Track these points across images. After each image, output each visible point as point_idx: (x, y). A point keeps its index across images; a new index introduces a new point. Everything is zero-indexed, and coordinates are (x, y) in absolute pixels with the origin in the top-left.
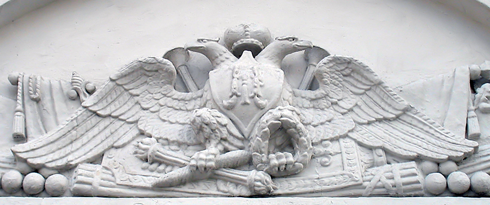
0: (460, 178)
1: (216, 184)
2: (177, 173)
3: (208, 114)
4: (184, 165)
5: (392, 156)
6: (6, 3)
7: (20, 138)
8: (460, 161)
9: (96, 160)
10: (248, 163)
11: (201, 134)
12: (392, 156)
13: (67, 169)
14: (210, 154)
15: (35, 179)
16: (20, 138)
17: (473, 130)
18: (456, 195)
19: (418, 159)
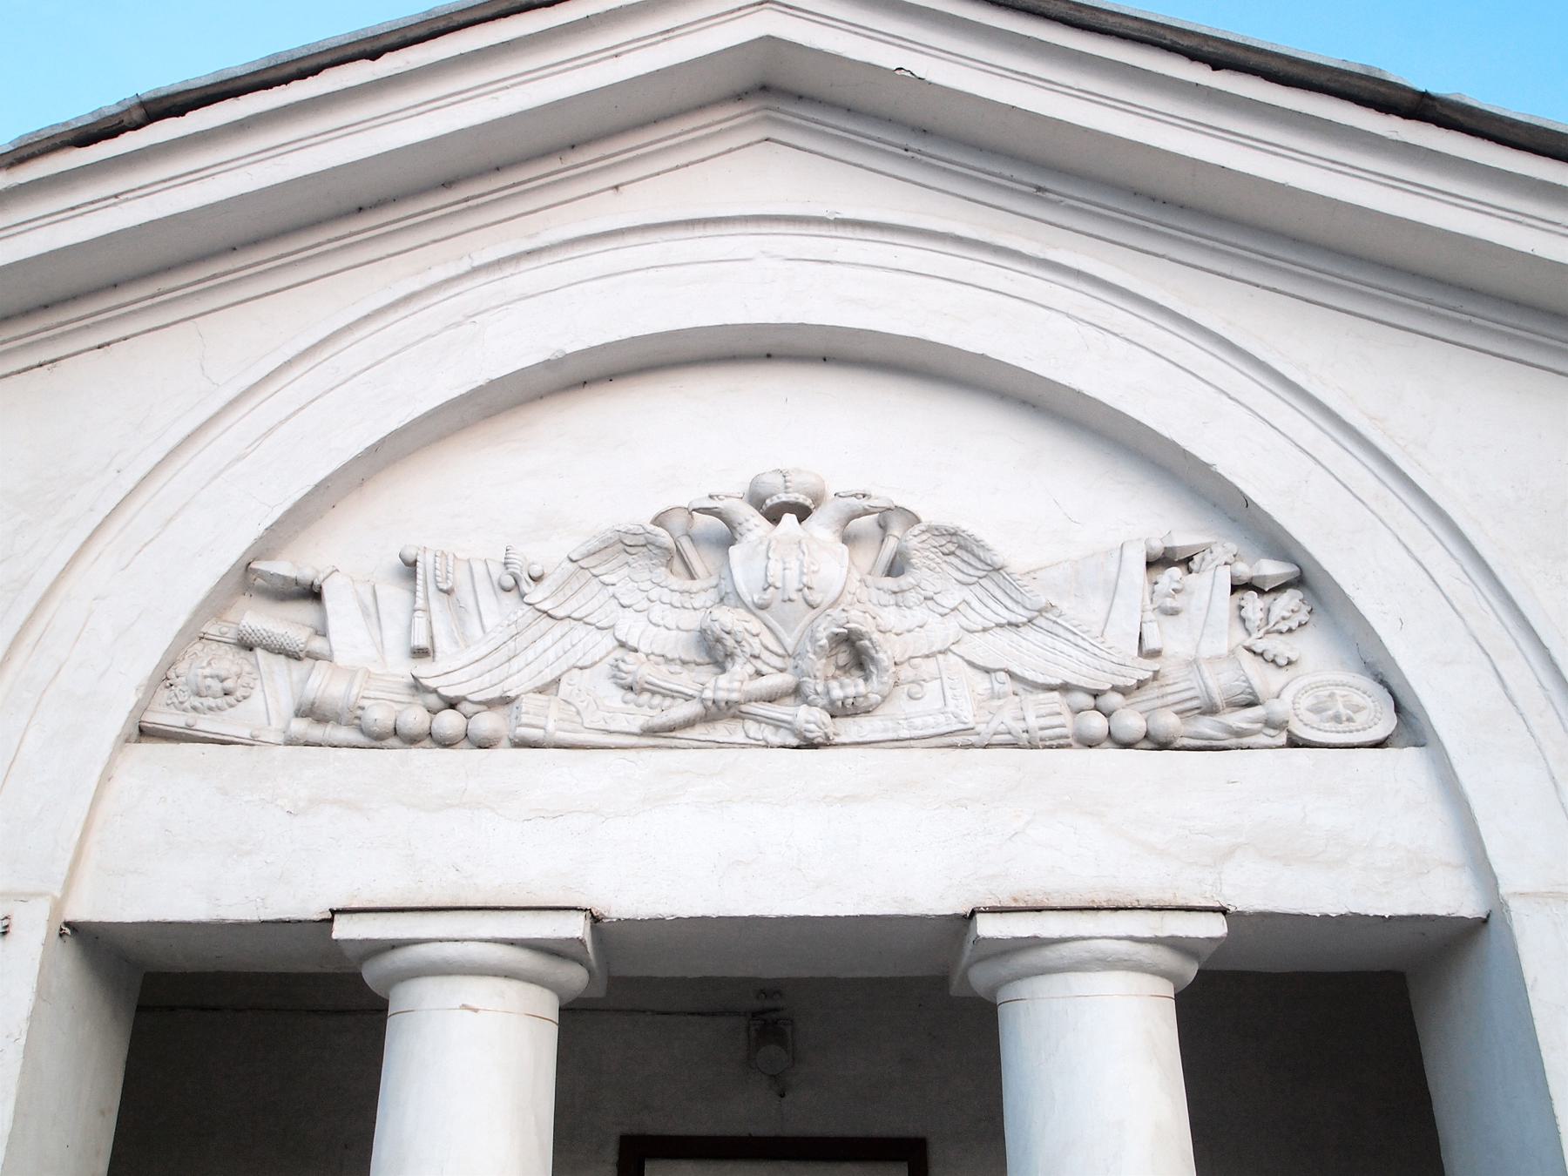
0: (1132, 722)
4: (688, 698)
7: (420, 653)
15: (449, 722)
19: (1065, 688)
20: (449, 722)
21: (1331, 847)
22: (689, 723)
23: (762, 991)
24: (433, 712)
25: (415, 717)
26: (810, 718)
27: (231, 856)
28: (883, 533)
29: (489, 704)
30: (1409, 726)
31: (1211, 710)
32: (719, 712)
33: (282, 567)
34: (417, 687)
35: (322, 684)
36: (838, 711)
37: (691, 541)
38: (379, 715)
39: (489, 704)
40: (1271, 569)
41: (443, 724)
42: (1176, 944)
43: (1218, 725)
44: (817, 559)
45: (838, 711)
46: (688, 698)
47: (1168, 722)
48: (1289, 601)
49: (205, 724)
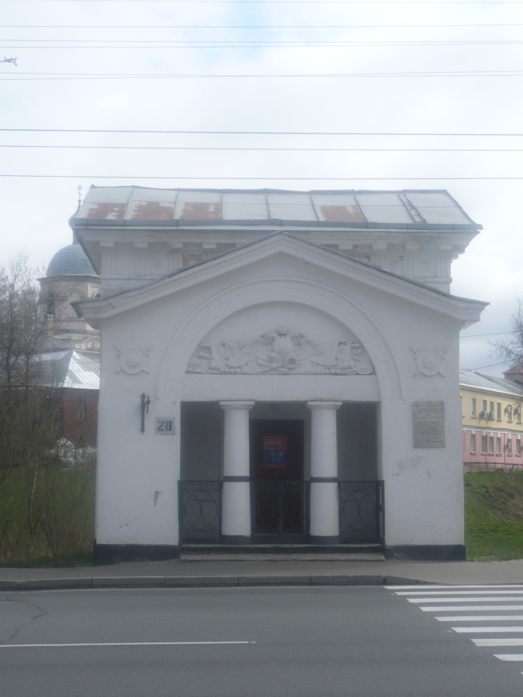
0: (333, 371)
1: (269, 215)
2: (267, 369)
3: (274, 355)
4: (267, 367)
5: (317, 365)
6: (510, 626)
7: (227, 359)
8: (333, 366)
9: (247, 364)
10: (283, 366)
11: (272, 360)
12: (317, 365)
13: (239, 367)
14: (274, 365)
15: (232, 370)
16: (227, 359)
17: (338, 357)
18: (331, 375)
19: (324, 365)
20: (232, 370)
21: (357, 391)
22: (268, 371)
23: (148, 402)
24: (230, 369)
25: (227, 370)
26: (285, 370)
27: (205, 389)
28: (299, 340)
29: (238, 367)
30: (373, 373)
31: (345, 369)
32: (272, 369)
33: (205, 345)
34: (227, 365)
35: (214, 364)
36: (289, 369)
37: (267, 340)
38: (222, 369)
39: (238, 367)
40: (357, 345)
41: (231, 371)
42: (334, 405)
43: (343, 373)
44: (285, 344)
45: (289, 369)
46: (267, 367)
47: (339, 371)
48: (359, 351)
49: (196, 370)
